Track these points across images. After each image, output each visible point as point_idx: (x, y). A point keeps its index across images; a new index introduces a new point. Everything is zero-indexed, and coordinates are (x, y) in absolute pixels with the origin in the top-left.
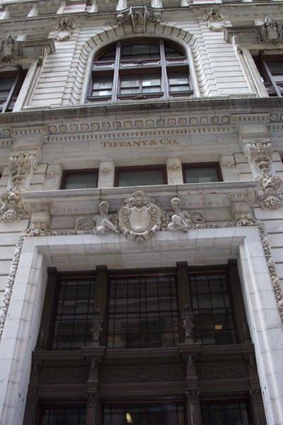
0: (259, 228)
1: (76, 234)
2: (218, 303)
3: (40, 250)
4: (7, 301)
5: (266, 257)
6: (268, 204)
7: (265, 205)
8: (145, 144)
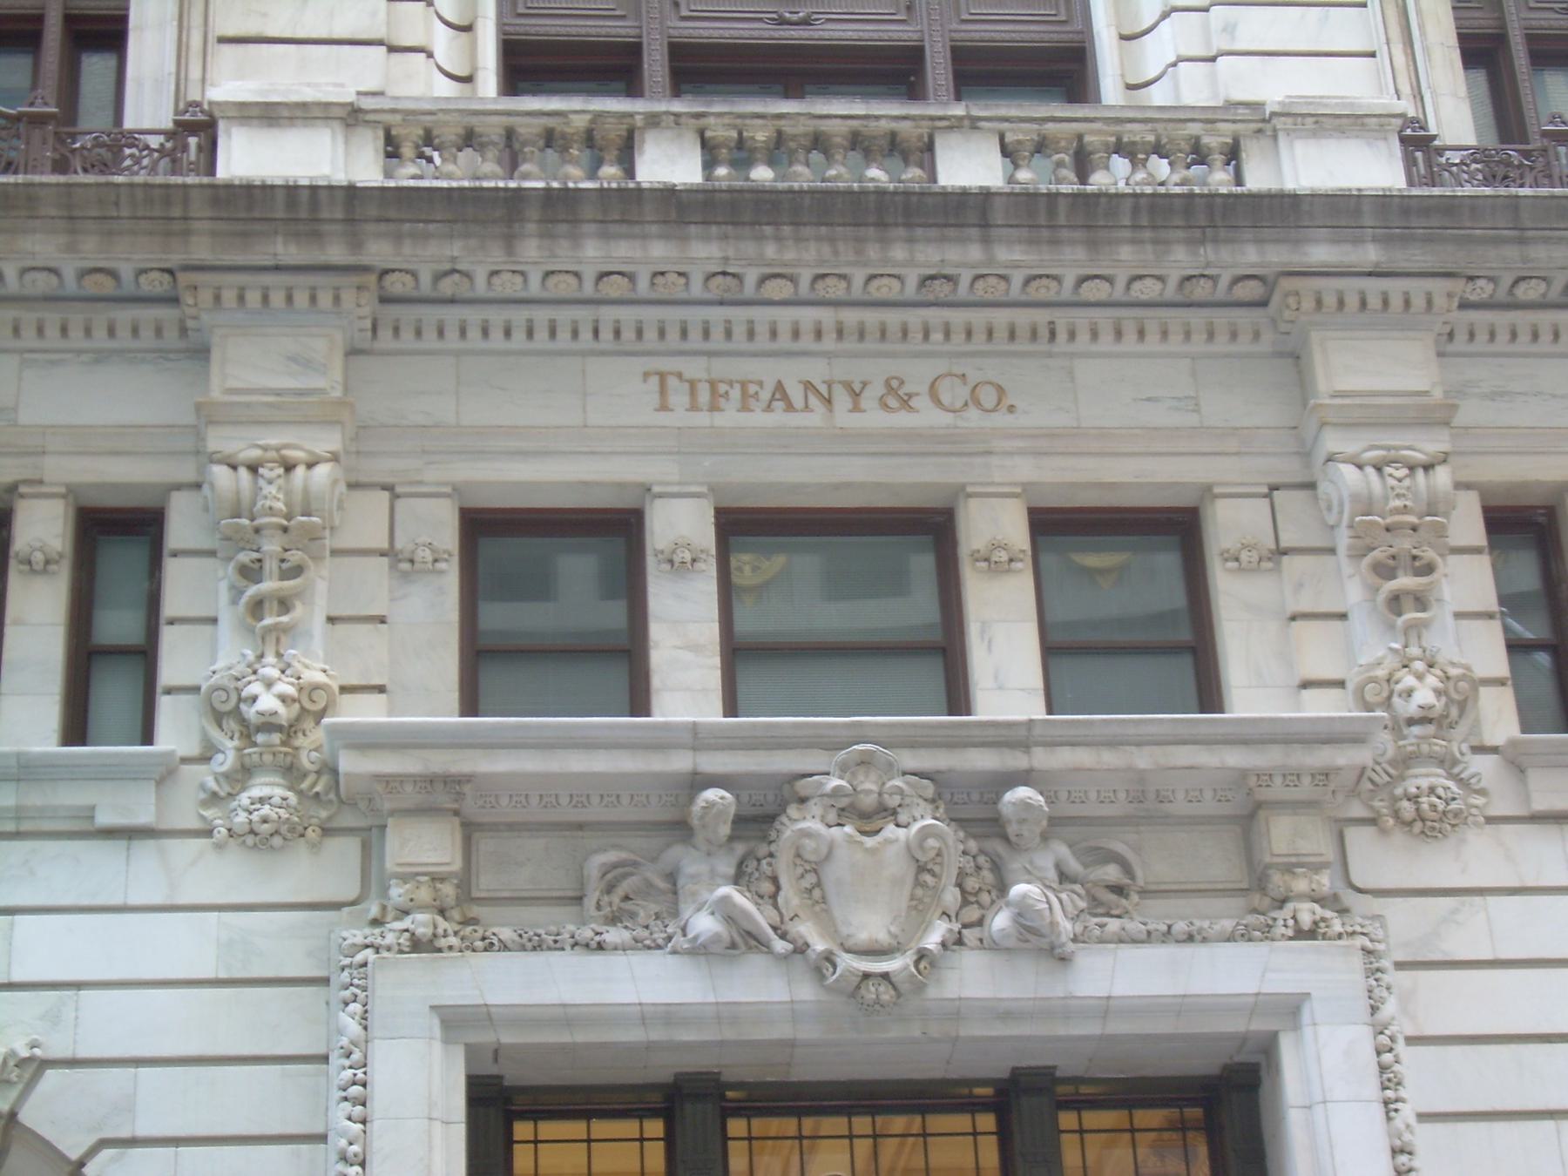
0: (1368, 952)
1: (600, 947)
2: (1103, 200)
3: (453, 1021)
5: (1386, 1103)
6: (1407, 808)
7: (1396, 814)
8: (856, 395)
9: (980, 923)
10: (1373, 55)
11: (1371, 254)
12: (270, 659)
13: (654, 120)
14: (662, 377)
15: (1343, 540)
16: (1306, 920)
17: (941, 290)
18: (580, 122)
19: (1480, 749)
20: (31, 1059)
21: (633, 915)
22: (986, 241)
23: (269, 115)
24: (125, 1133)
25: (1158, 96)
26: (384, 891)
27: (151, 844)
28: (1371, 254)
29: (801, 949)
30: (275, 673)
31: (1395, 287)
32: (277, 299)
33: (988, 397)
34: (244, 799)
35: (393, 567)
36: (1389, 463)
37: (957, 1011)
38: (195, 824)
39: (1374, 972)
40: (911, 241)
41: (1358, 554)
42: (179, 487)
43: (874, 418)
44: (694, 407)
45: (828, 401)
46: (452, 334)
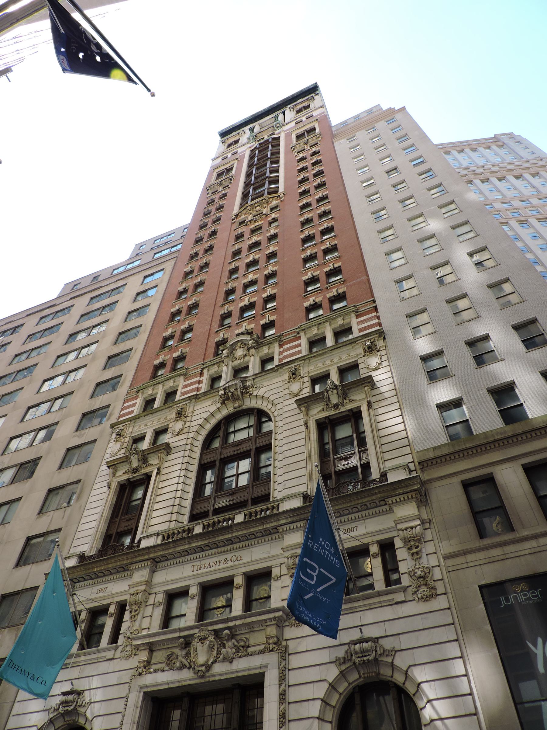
42: (395, 537)
43: (222, 566)
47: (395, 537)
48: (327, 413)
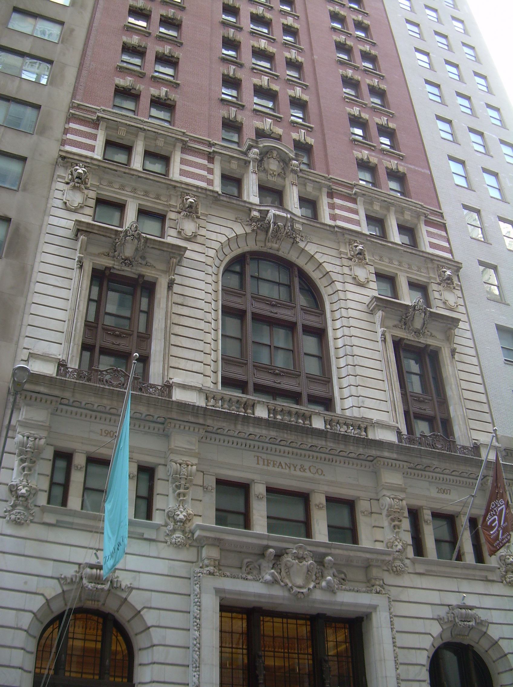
0: (389, 598)
3: (218, 591)
4: (198, 645)
5: (392, 628)
7: (392, 570)
8: (295, 467)
9: (319, 583)
10: (388, 412)
11: (395, 456)
12: (181, 507)
13: (259, 402)
14: (258, 457)
15: (385, 513)
16: (378, 590)
17: (314, 448)
18: (245, 400)
19: (407, 558)
20: (130, 587)
21: (252, 573)
22: (326, 441)
23: (184, 387)
24: (149, 606)
25: (348, 413)
26: (202, 560)
27: (154, 543)
28: (395, 456)
29: (286, 585)
30: (183, 510)
31: (398, 462)
32: (187, 428)
33: (320, 472)
34: (174, 536)
35: (204, 488)
36: (395, 498)
37: (314, 601)
38: (163, 540)
39: (390, 602)
40: (312, 438)
41: (388, 516)
42: (160, 464)
43: (298, 473)
44: (264, 465)
45: (290, 468)
46: (217, 441)
47: (160, 464)
48: (406, 334)
